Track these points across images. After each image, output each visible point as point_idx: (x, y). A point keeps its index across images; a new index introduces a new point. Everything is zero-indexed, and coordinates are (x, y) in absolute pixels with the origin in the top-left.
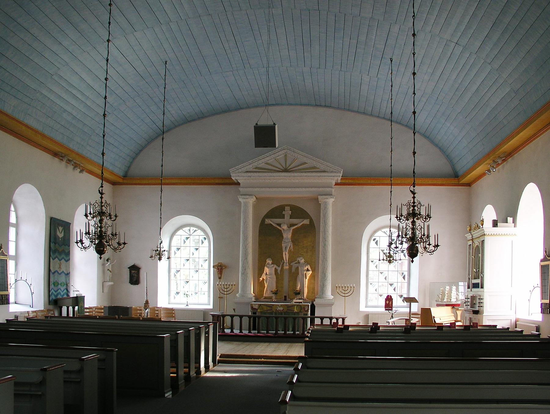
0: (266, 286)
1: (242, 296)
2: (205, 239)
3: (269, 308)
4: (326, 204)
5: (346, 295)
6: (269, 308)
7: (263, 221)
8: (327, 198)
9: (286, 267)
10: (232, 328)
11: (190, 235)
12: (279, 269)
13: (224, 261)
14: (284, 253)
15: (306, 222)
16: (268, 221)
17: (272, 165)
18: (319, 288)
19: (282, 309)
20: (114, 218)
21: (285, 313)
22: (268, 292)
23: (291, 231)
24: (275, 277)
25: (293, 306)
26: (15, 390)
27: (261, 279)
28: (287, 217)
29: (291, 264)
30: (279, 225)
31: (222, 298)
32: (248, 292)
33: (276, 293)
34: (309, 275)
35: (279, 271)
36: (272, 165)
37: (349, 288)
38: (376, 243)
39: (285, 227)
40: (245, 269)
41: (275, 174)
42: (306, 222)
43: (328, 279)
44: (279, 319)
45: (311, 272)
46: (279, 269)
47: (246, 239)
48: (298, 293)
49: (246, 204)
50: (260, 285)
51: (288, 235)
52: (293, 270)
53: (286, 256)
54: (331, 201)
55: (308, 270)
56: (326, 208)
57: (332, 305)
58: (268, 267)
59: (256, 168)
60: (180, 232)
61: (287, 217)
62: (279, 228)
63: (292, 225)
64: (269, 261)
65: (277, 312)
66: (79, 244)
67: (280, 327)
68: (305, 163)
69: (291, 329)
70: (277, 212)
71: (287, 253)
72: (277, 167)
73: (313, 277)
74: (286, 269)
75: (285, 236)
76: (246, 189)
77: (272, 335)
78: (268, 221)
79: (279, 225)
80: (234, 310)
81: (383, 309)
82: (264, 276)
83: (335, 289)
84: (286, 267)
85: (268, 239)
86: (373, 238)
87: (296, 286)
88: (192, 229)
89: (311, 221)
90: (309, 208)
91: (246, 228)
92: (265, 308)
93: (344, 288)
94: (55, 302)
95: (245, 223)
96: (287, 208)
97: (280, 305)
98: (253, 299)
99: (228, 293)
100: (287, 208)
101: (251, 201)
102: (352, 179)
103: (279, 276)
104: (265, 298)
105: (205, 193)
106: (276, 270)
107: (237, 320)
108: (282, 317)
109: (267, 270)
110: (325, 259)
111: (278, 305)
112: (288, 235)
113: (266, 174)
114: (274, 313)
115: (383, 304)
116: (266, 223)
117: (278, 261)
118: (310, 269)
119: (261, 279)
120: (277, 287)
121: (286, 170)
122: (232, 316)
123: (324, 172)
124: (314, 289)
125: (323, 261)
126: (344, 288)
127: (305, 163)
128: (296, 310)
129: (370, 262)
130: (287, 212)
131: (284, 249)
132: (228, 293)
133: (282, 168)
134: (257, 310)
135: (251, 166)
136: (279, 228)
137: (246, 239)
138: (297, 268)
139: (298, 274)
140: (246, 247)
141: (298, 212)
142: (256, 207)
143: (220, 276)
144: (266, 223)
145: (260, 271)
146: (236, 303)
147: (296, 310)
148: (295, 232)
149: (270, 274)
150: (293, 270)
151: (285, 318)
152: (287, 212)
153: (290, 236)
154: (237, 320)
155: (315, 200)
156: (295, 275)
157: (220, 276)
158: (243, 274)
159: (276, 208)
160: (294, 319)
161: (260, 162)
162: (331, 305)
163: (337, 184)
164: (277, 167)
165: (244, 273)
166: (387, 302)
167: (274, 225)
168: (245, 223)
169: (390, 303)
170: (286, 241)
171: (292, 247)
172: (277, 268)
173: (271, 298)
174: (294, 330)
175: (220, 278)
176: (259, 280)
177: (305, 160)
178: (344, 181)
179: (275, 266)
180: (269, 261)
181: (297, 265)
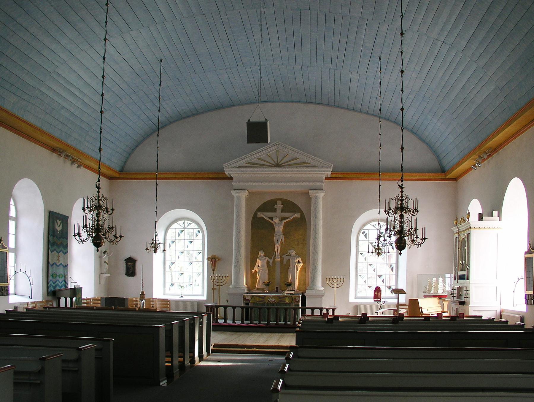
0: (258, 277)
1: (235, 287)
2: (199, 232)
3: (261, 299)
4: (316, 198)
5: (336, 287)
6: (261, 299)
7: (255, 214)
8: (318, 193)
9: (278, 259)
10: (225, 319)
11: (185, 228)
12: (271, 261)
13: (217, 254)
14: (276, 246)
15: (297, 215)
16: (260, 215)
17: (264, 160)
18: (310, 280)
19: (274, 300)
20: (110, 212)
21: (277, 304)
22: (261, 283)
23: (283, 224)
24: (267, 269)
25: (285, 297)
26: (14, 379)
27: (254, 271)
28: (279, 210)
29: (283, 256)
30: (271, 218)
31: (215, 289)
32: (241, 284)
33: (268, 284)
34: (300, 267)
35: (271, 264)
36: (264, 160)
37: (339, 280)
38: (365, 236)
39: (277, 220)
40: (238, 262)
41: (267, 169)
42: (297, 215)
43: (318, 271)
44: (271, 310)
45: (302, 264)
46: (271, 261)
47: (238, 232)
48: (289, 285)
49: (239, 198)
50: (253, 277)
51: (279, 228)
52: (285, 262)
53: (277, 248)
54: (321, 195)
55: (299, 262)
56: (316, 202)
57: (323, 296)
58: (260, 260)
59: (249, 163)
60: (175, 225)
61: (279, 210)
62: (271, 221)
63: (283, 219)
64: (261, 254)
65: (269, 303)
66: (77, 237)
67: (272, 317)
68: (296, 158)
69: (282, 319)
70: (269, 206)
71: (278, 246)
72: (269, 162)
73: (304, 269)
74: (278, 262)
75: (276, 229)
76: (238, 184)
77: (264, 326)
78: (260, 215)
79: (271, 218)
80: (227, 301)
81: (372, 300)
82: (256, 268)
83: (325, 281)
84: (278, 259)
85: (260, 232)
86: (363, 231)
87: (287, 278)
88: (187, 222)
89: (302, 214)
90: (300, 202)
91: (238, 221)
92: (257, 299)
93: (334, 280)
94: (53, 293)
95: (238, 216)
96: (279, 202)
97: (272, 297)
98: (246, 291)
99: (221, 284)
100: (279, 202)
101: (244, 195)
102: (342, 174)
103: (270, 268)
104: (258, 289)
105: (199, 188)
106: (268, 262)
107: (230, 311)
108: (274, 308)
109: (259, 262)
110: (316, 251)
111: (270, 296)
112: (279, 228)
113: (258, 169)
114: (266, 304)
115: (372, 295)
116: (258, 216)
117: (270, 253)
118: (301, 261)
119: (254, 271)
120: (269, 279)
121: (277, 165)
122: (225, 307)
123: (315, 167)
124: (305, 280)
125: (313, 253)
126: (334, 280)
127: (296, 158)
128: (287, 301)
129: (360, 255)
130: (279, 206)
131: (275, 242)
132: (221, 284)
133: (273, 163)
134: (250, 301)
135: (244, 161)
136: (271, 221)
137: (238, 232)
138: (289, 261)
139: (289, 266)
140: (239, 239)
141: (289, 206)
142: (248, 201)
143: (213, 268)
144: (258, 216)
145: (253, 263)
146: (229, 294)
147: (287, 301)
148: (286, 226)
149: (262, 266)
150: (285, 262)
151: (277, 309)
152: (279, 206)
153: (281, 229)
154: (230, 311)
155: (306, 194)
156: (286, 267)
157: (213, 268)
158: (236, 266)
159: (268, 202)
160: (286, 309)
161: (253, 157)
162: (321, 296)
163: (327, 179)
164: (269, 162)
165: (237, 265)
166: (376, 293)
167: (266, 218)
168: (238, 216)
169: (379, 294)
170: (278, 234)
171: (283, 240)
172: (269, 260)
173: (263, 289)
174: (285, 320)
175: (213, 270)
176: (251, 272)
177: (296, 155)
178: (334, 176)
179: (267, 258)
180: (261, 254)
181: (289, 257)
